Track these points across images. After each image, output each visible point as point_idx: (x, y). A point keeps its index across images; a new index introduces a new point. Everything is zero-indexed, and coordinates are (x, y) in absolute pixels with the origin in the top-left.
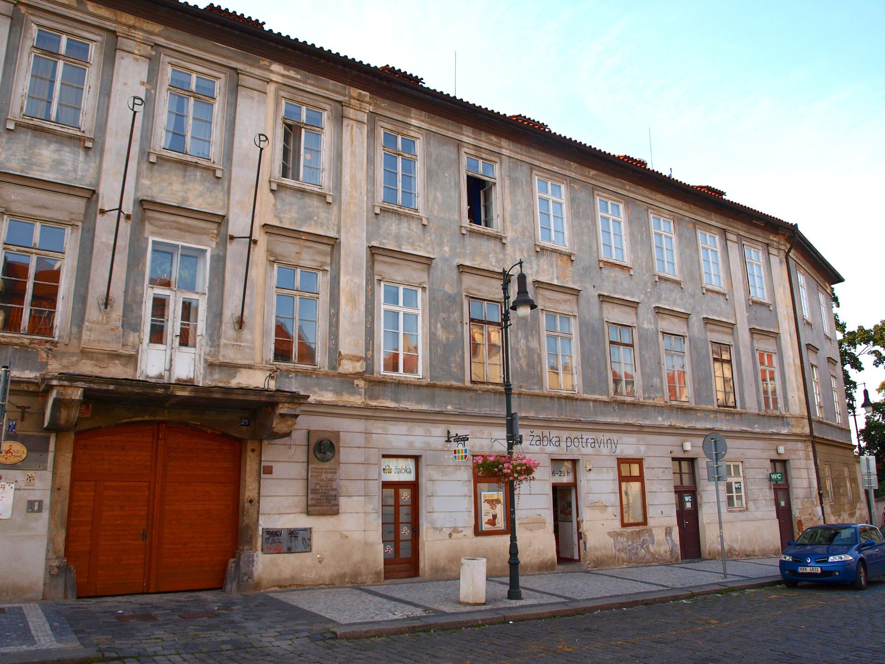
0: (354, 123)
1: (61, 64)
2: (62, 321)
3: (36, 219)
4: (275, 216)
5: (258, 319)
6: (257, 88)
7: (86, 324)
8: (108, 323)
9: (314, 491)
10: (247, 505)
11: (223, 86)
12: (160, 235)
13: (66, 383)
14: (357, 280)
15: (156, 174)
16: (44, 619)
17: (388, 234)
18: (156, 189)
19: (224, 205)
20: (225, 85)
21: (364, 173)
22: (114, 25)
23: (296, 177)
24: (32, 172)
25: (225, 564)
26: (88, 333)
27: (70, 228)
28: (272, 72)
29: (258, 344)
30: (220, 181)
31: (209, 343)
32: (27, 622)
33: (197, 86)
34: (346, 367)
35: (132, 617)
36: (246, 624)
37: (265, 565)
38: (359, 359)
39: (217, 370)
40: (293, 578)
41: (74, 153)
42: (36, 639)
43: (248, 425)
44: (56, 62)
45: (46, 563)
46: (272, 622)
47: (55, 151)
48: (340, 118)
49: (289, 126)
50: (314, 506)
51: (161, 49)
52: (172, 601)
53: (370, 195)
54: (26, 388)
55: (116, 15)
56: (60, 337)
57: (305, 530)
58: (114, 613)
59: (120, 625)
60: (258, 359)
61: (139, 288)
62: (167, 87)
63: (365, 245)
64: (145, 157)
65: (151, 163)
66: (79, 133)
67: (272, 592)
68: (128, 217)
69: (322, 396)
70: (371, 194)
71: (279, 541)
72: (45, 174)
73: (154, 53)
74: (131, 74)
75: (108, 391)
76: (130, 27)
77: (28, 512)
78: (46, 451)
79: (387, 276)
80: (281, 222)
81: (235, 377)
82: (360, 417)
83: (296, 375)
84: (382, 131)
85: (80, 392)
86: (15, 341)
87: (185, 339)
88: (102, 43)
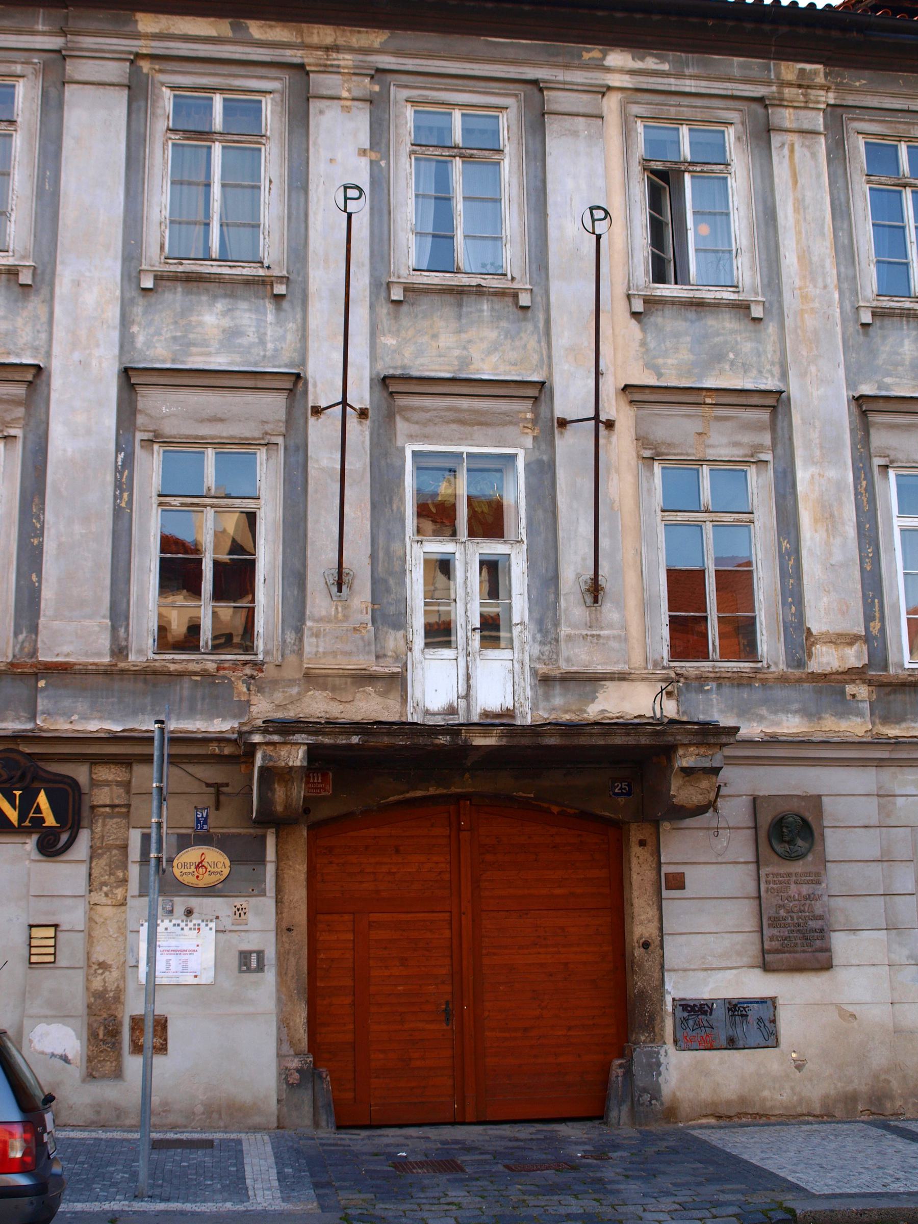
0: (795, 137)
1: (217, 149)
2: (266, 623)
3: (204, 442)
4: (647, 366)
5: (631, 578)
6: (582, 110)
7: (309, 623)
8: (346, 618)
9: (775, 922)
10: (638, 952)
11: (514, 122)
12: (426, 438)
13: (276, 738)
14: (832, 473)
15: (405, 322)
16: (271, 1160)
17: (896, 365)
18: (408, 352)
19: (541, 360)
20: (519, 120)
21: (829, 241)
22: (300, 53)
23: (681, 277)
24: (191, 359)
25: (606, 1069)
26: (314, 640)
27: (264, 450)
28: (608, 70)
29: (635, 630)
30: (530, 313)
31: (539, 637)
32: (243, 1164)
33: (466, 131)
34: (824, 660)
35: (421, 1165)
36: (622, 1187)
37: (684, 1073)
38: (851, 640)
39: (558, 689)
40: (743, 1100)
41: (257, 311)
42: (251, 1193)
43: (629, 794)
44: (210, 148)
45: (279, 1064)
46: (674, 1184)
47: (224, 314)
48: (762, 135)
49: (663, 175)
50: (777, 951)
51: (389, 77)
52: (502, 1138)
53: (845, 286)
54: (217, 751)
55: (300, 33)
56: (267, 653)
57: (762, 1001)
58: (391, 1156)
59: (397, 1177)
60: (637, 659)
61: (396, 546)
62: (409, 148)
63: (844, 395)
64: (383, 294)
65: (393, 302)
66: (261, 272)
67: (701, 1127)
68: (363, 414)
69: (778, 724)
70: (849, 282)
71: (708, 1024)
72: (212, 359)
73: (377, 88)
74: (339, 140)
75: (350, 747)
76: (327, 49)
77: (241, 971)
78: (262, 861)
79: (900, 456)
80: (660, 375)
81: (593, 701)
82: (863, 763)
83: (719, 686)
84: (861, 142)
85: (301, 752)
86: (192, 667)
87: (491, 629)
88: (282, 94)
